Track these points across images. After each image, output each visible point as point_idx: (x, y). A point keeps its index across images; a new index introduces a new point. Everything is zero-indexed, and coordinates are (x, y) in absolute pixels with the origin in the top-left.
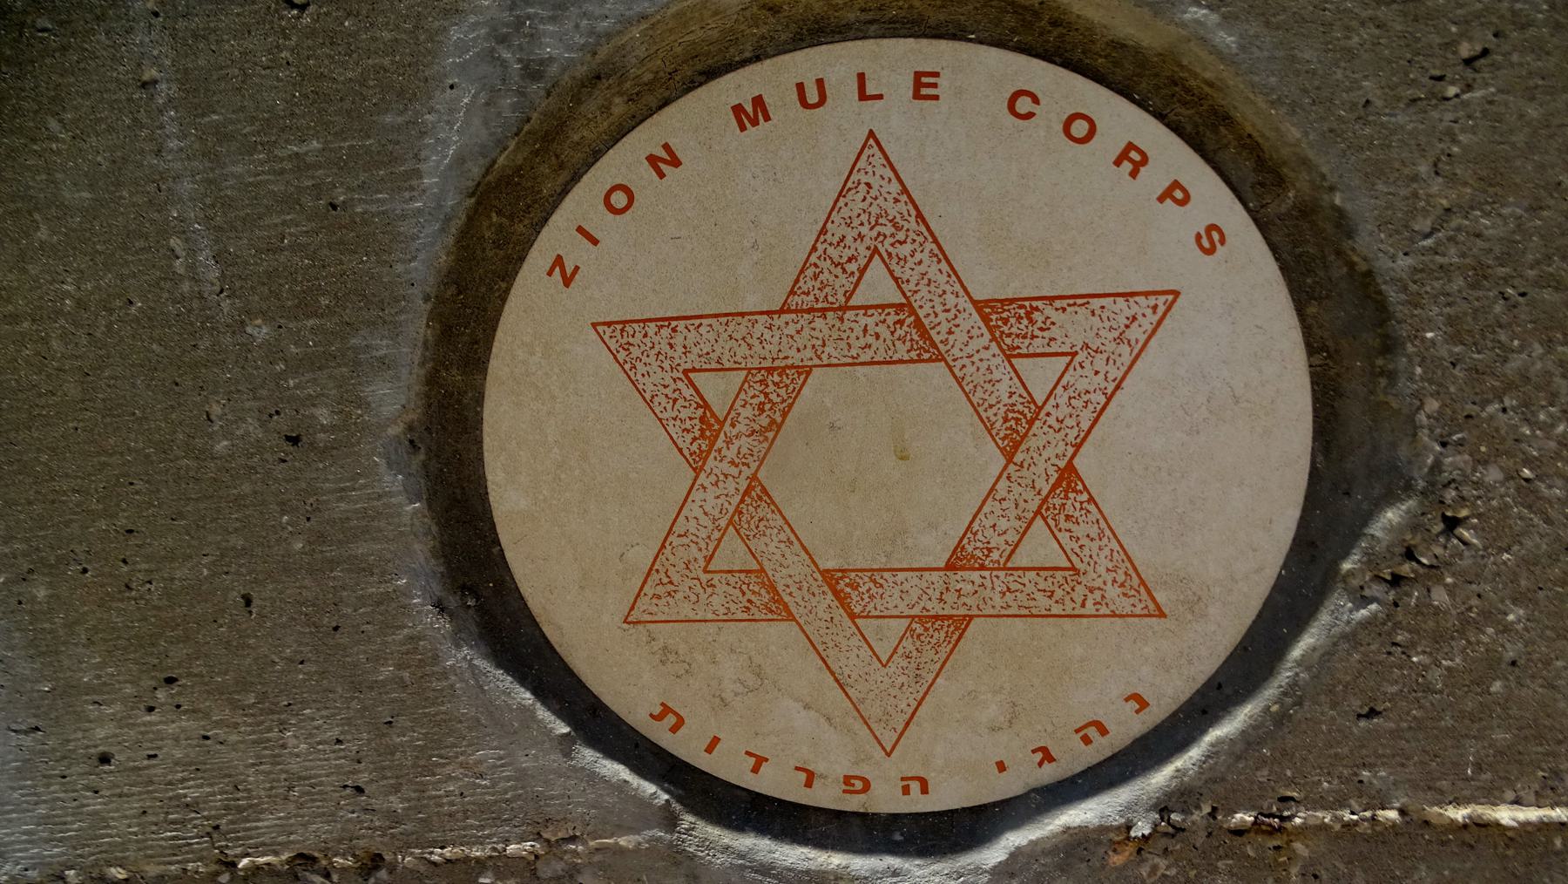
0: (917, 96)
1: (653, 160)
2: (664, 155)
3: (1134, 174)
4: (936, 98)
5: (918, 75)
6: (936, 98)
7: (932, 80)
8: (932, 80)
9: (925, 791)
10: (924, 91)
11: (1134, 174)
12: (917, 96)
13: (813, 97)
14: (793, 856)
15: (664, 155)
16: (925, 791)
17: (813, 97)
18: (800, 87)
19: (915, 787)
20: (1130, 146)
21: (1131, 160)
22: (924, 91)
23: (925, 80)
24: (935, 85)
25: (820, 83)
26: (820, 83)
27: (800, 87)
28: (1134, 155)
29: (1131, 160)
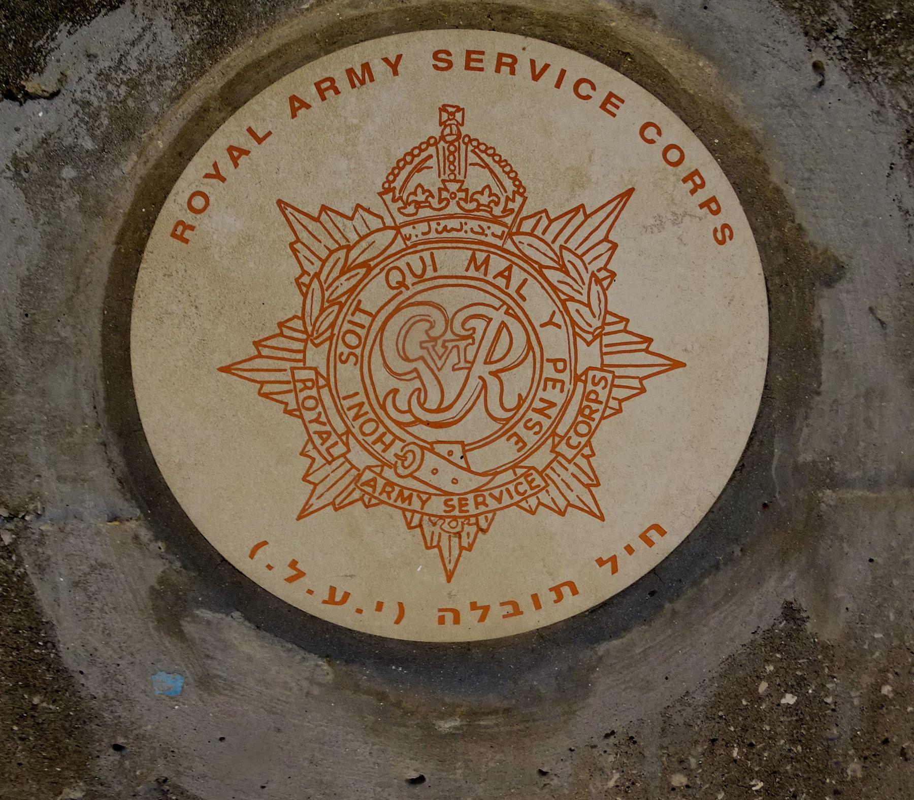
6: (614, 115)
9: (662, 532)
16: (662, 532)
19: (654, 535)
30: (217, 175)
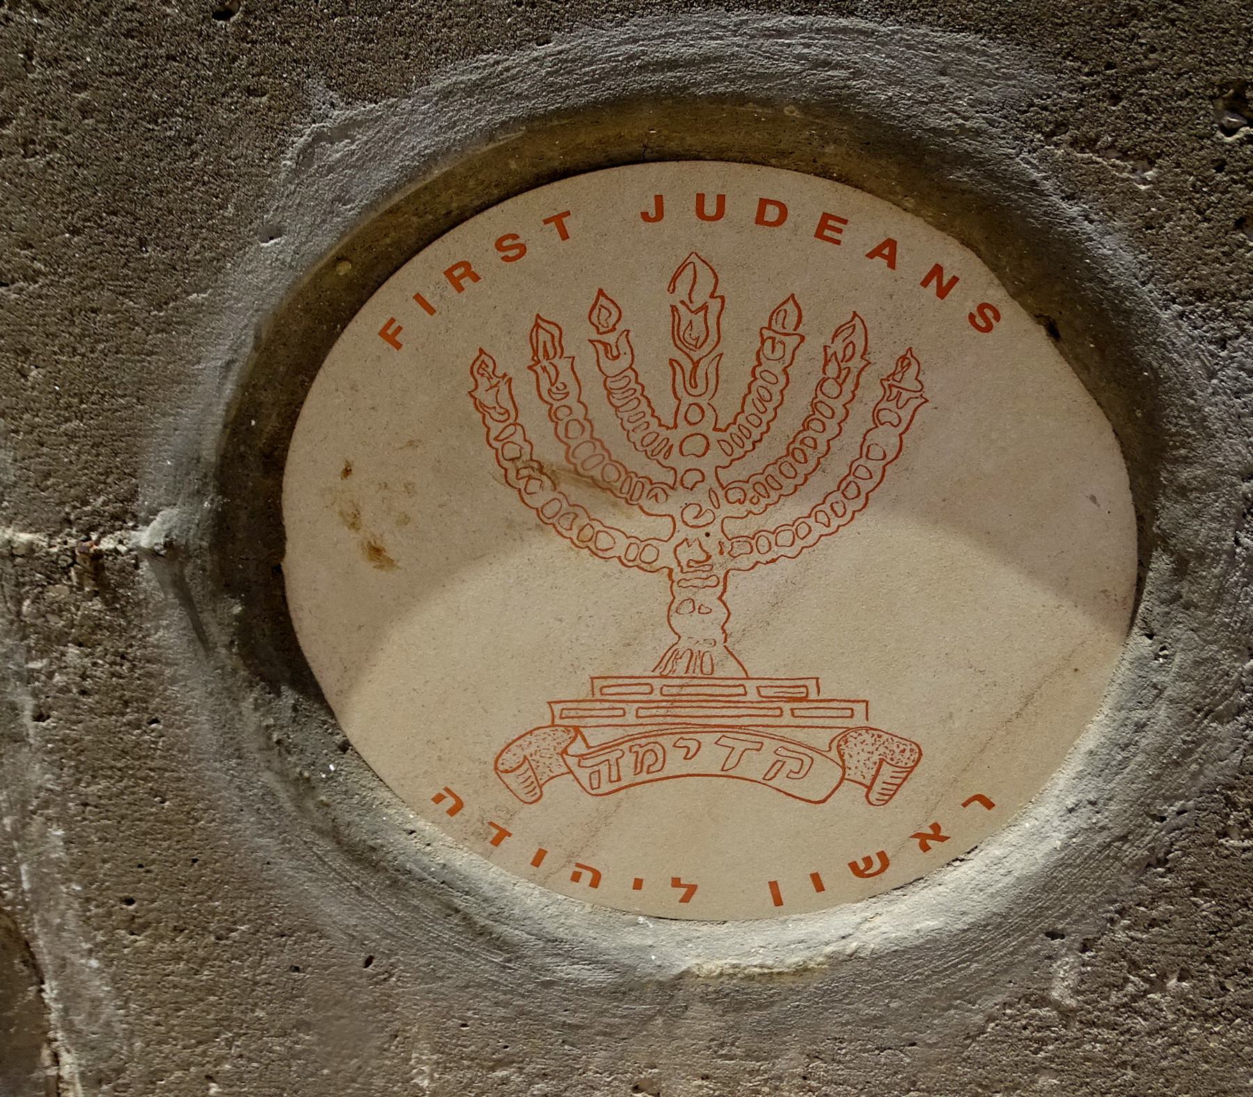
0: (819, 234)
1: (937, 270)
2: (934, 282)
3: (476, 278)
4: (838, 242)
5: (826, 217)
7: (838, 225)
8: (838, 225)
10: (827, 233)
11: (476, 278)
12: (819, 234)
13: (710, 209)
14: (789, 47)
15: (934, 282)
17: (710, 209)
18: (700, 198)
20: (449, 273)
21: (462, 276)
22: (827, 233)
23: (831, 223)
24: (840, 231)
25: (721, 199)
26: (721, 199)
27: (700, 198)
28: (456, 273)
29: (462, 276)
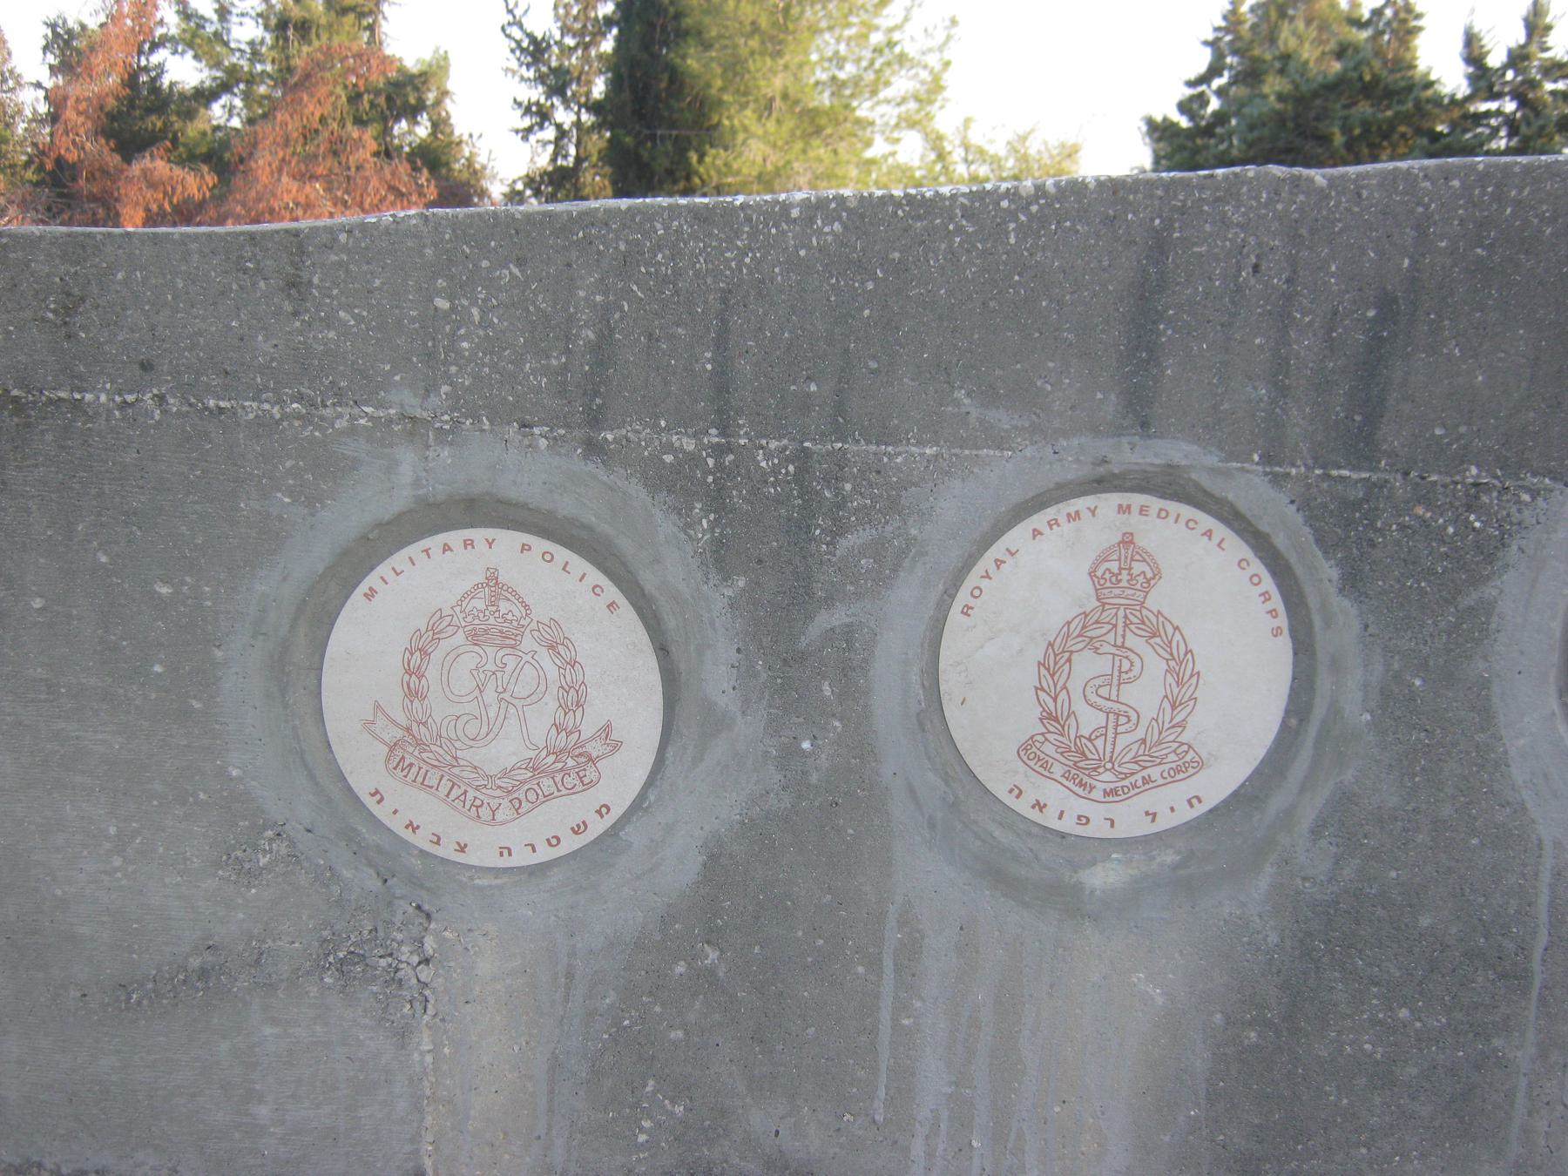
30: (988, 576)
